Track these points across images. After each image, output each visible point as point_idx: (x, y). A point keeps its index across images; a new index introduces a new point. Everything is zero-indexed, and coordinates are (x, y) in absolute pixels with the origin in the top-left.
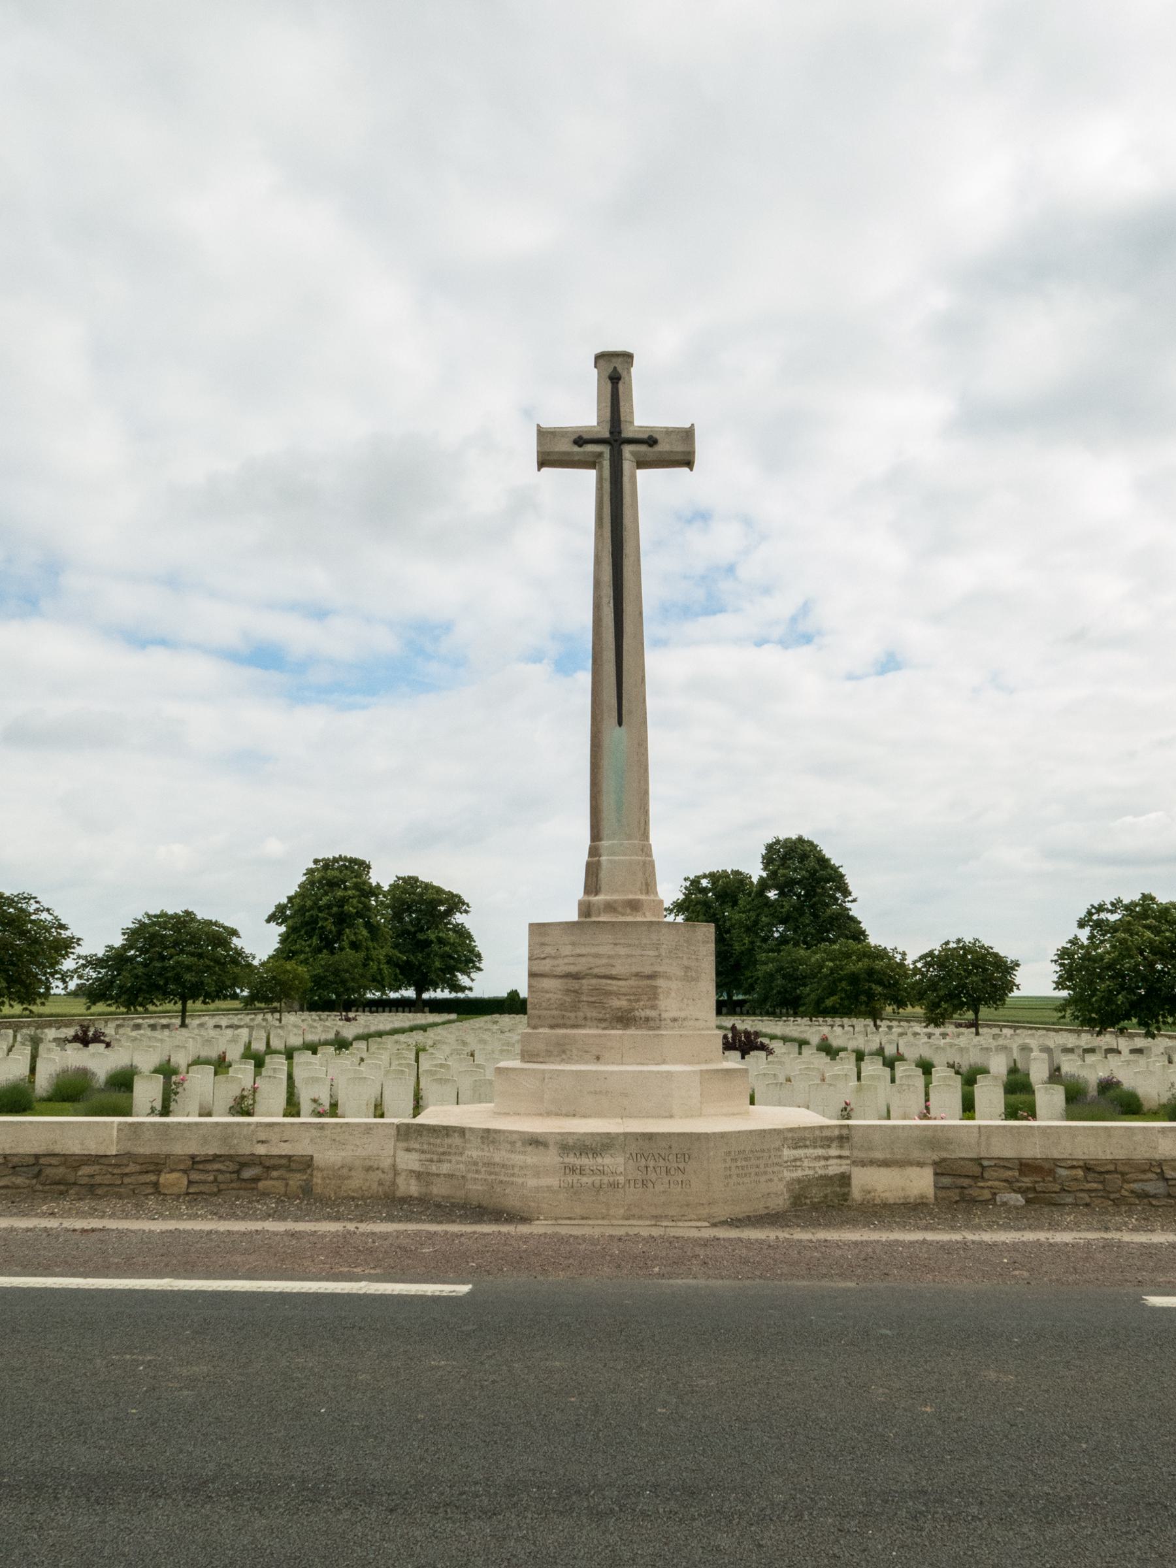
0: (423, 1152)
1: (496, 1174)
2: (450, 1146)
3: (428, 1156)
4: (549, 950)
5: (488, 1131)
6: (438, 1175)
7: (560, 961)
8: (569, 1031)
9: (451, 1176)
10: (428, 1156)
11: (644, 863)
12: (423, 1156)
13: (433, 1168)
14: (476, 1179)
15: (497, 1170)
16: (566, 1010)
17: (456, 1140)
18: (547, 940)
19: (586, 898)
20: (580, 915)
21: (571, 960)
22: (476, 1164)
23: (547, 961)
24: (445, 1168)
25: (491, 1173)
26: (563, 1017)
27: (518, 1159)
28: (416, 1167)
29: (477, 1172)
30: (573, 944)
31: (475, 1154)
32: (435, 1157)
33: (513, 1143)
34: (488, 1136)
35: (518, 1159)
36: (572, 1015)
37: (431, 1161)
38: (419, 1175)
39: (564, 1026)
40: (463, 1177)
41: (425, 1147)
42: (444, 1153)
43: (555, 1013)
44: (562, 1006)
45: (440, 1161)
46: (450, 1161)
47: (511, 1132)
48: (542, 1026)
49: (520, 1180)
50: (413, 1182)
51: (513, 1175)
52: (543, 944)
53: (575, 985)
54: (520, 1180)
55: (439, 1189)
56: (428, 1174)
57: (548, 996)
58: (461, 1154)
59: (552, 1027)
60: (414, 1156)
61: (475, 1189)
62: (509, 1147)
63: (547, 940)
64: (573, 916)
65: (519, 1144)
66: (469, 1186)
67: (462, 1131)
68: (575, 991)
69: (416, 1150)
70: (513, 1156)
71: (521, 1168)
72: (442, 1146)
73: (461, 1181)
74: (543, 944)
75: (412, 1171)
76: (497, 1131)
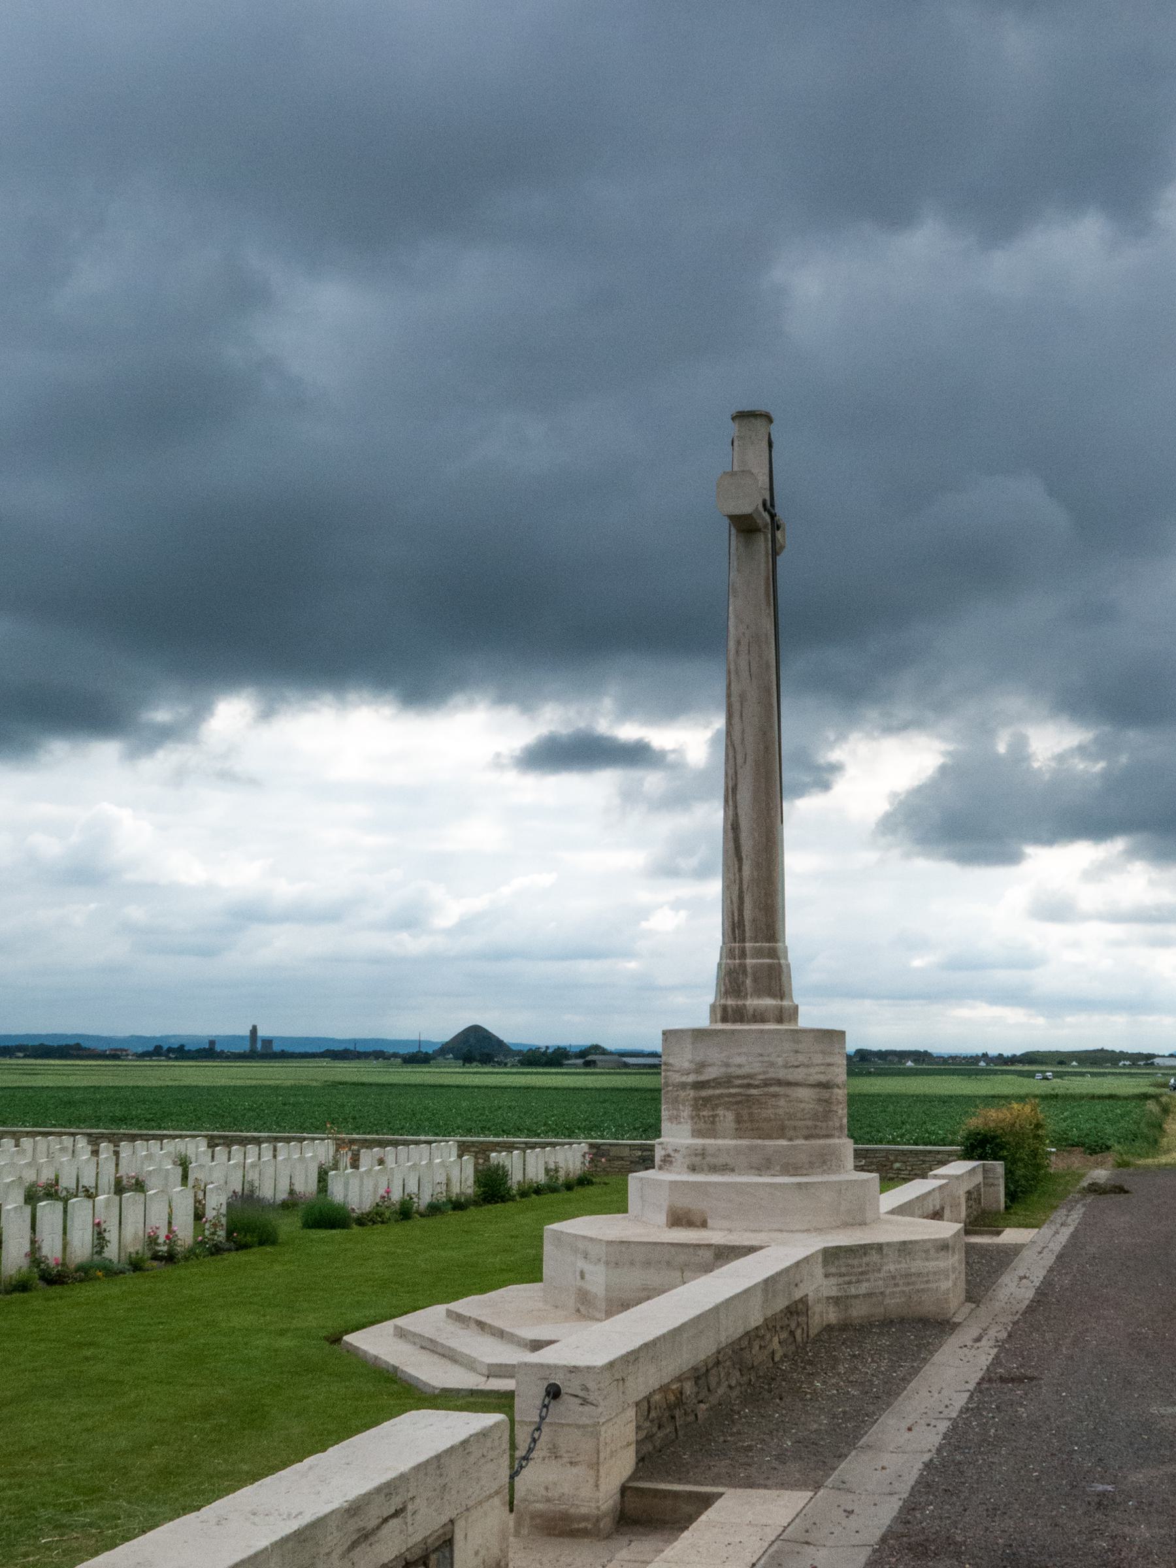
0: (841, 1275)
1: (913, 1283)
2: (867, 1265)
3: (847, 1278)
4: (801, 1058)
5: (904, 1243)
6: (856, 1297)
7: (812, 1070)
8: (821, 1142)
9: (869, 1295)
10: (847, 1278)
11: (770, 966)
12: (841, 1280)
13: (853, 1291)
14: (893, 1293)
15: (913, 1279)
16: (818, 1120)
17: (874, 1257)
18: (800, 1047)
19: (723, 1002)
20: (713, 1020)
21: (822, 1068)
22: (894, 1278)
23: (799, 1070)
24: (864, 1288)
25: (909, 1284)
26: (816, 1126)
27: (931, 1265)
28: (834, 1292)
29: (896, 1285)
30: (823, 1052)
31: (892, 1267)
32: (854, 1279)
33: (927, 1251)
34: (905, 1248)
35: (931, 1265)
36: (824, 1125)
37: (850, 1283)
38: (836, 1301)
39: (818, 1137)
40: (882, 1293)
41: (843, 1270)
42: (862, 1273)
43: (810, 1123)
44: (815, 1117)
45: (858, 1281)
46: (868, 1280)
47: (924, 1241)
48: (797, 1137)
49: (934, 1286)
50: (831, 1309)
51: (927, 1282)
52: (797, 1052)
53: (825, 1094)
54: (934, 1286)
55: (859, 1311)
56: (847, 1297)
57: (802, 1105)
58: (879, 1270)
59: (807, 1138)
60: (833, 1281)
61: (894, 1303)
62: (924, 1255)
63: (800, 1047)
64: (703, 1021)
65: (932, 1252)
66: (887, 1301)
67: (879, 1247)
68: (826, 1101)
69: (833, 1275)
70: (927, 1264)
71: (935, 1273)
72: (861, 1266)
73: (880, 1298)
74: (797, 1052)
75: (828, 1298)
76: (911, 1242)
